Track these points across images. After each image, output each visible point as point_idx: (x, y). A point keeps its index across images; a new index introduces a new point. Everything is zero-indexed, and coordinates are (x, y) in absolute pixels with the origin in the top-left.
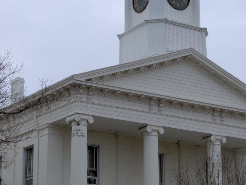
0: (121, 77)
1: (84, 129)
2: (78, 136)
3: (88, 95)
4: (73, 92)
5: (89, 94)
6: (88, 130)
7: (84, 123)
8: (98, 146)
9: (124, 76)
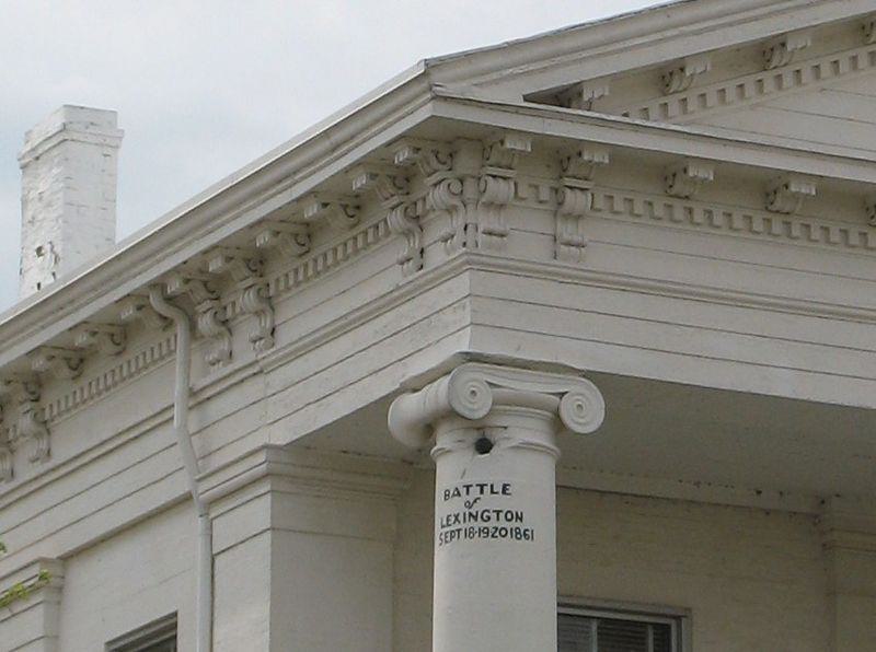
0: (826, 70)
1: (527, 477)
2: (484, 532)
3: (555, 214)
4: (438, 196)
5: (566, 208)
6: (561, 489)
7: (532, 431)
8: (678, 618)
9: (844, 66)
